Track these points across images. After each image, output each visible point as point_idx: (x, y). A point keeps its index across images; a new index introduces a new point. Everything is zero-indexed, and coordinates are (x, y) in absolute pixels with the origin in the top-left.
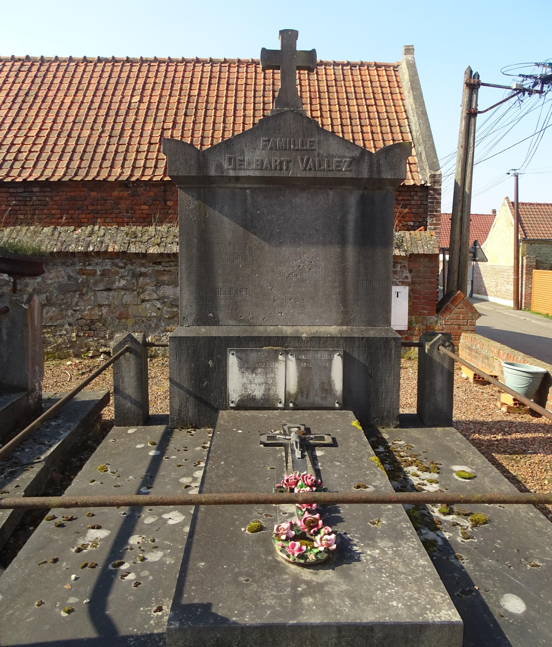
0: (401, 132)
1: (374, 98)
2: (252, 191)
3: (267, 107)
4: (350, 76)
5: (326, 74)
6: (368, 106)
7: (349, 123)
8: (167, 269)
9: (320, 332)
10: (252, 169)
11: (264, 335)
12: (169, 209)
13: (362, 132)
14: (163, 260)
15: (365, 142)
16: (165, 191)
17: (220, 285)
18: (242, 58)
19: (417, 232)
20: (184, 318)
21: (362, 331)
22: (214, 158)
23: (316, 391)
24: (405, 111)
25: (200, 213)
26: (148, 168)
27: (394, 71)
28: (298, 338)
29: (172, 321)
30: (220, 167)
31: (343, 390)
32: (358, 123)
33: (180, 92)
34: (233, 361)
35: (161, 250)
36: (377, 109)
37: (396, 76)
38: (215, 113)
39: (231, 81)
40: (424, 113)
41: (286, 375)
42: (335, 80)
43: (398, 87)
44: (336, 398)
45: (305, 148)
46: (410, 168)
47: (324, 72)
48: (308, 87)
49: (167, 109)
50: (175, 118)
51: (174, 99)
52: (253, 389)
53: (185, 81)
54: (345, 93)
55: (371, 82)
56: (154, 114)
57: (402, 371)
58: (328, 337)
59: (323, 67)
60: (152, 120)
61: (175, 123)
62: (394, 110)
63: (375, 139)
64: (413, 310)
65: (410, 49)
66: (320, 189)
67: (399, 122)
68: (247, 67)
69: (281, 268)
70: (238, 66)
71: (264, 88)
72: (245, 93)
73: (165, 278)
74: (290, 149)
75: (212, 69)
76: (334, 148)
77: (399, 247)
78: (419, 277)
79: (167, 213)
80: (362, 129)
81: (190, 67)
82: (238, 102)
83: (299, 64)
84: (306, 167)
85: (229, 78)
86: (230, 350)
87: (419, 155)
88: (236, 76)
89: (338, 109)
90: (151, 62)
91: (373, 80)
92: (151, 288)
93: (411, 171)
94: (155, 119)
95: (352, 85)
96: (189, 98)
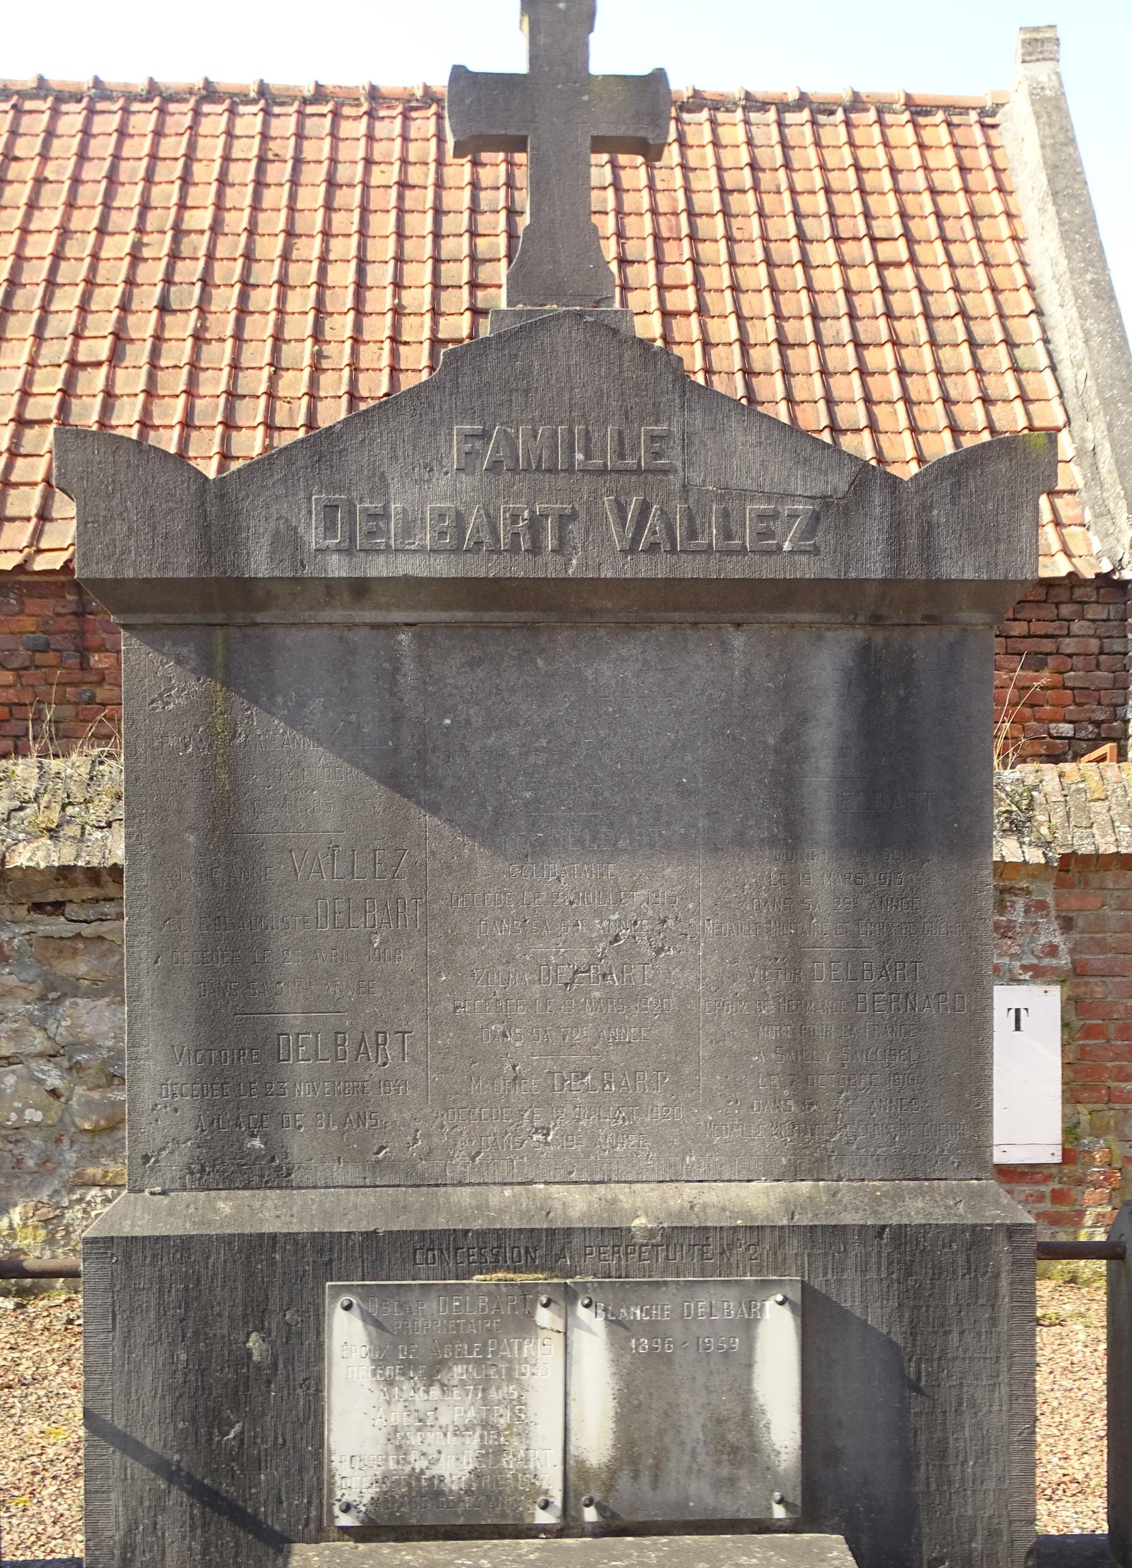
0: (1016, 369)
1: (907, 235)
2: (419, 638)
3: (485, 273)
4: (812, 151)
5: (716, 144)
6: (881, 266)
7: (810, 336)
8: (87, 930)
9: (704, 1207)
10: (421, 550)
11: (477, 1225)
12: (101, 682)
13: (863, 371)
14: (71, 893)
15: (876, 409)
16: (80, 613)
17: (295, 1019)
18: (388, 83)
19: (1085, 765)
20: (146, 1158)
21: (877, 1200)
22: (267, 506)
23: (694, 1454)
24: (1030, 286)
25: (210, 726)
26: (13, 519)
27: (983, 126)
28: (615, 1236)
29: (106, 1141)
30: (288, 541)
31: (803, 1455)
32: (847, 335)
33: (142, 217)
34: (347, 1335)
35: (62, 855)
36: (918, 277)
37: (989, 146)
38: (282, 299)
39: (343, 174)
40: (1105, 293)
41: (566, 1390)
42: (754, 166)
43: (1000, 189)
44: (777, 1484)
45: (631, 462)
46: (1054, 510)
47: (707, 137)
48: (645, 193)
49: (90, 283)
50: (121, 322)
51: (118, 246)
52: (432, 1452)
53: (162, 172)
54: (790, 218)
55: (894, 171)
56: (37, 303)
57: (1044, 1337)
58: (735, 1229)
59: (705, 114)
60: (31, 329)
61: (120, 338)
62: (984, 283)
63: (914, 396)
64: (1080, 1079)
65: (1043, 41)
66: (695, 624)
67: (1004, 328)
68: (406, 117)
69: (539, 948)
70: (370, 114)
71: (475, 199)
72: (400, 222)
73: (81, 967)
74: (570, 470)
75: (266, 124)
76: (747, 461)
77: (1016, 828)
78: (1103, 947)
79: (92, 700)
80: (860, 358)
81: (180, 117)
82: (370, 256)
83: (603, 130)
84: (635, 540)
85: (333, 160)
86: (338, 1291)
87: (1088, 455)
88: (361, 153)
89: (765, 281)
90: (23, 95)
91: (899, 164)
92: (21, 1008)
93: (1057, 523)
94: (41, 324)
95: (819, 184)
96: (176, 241)
